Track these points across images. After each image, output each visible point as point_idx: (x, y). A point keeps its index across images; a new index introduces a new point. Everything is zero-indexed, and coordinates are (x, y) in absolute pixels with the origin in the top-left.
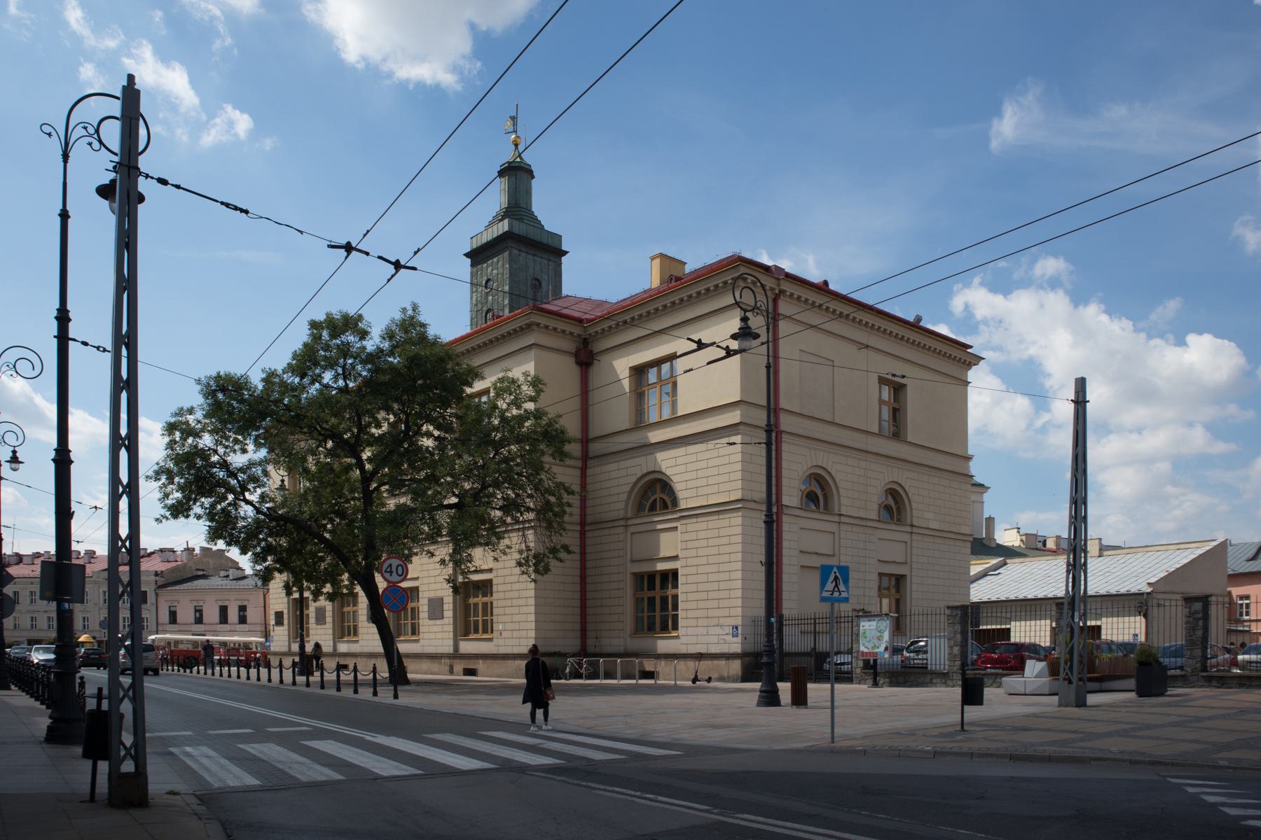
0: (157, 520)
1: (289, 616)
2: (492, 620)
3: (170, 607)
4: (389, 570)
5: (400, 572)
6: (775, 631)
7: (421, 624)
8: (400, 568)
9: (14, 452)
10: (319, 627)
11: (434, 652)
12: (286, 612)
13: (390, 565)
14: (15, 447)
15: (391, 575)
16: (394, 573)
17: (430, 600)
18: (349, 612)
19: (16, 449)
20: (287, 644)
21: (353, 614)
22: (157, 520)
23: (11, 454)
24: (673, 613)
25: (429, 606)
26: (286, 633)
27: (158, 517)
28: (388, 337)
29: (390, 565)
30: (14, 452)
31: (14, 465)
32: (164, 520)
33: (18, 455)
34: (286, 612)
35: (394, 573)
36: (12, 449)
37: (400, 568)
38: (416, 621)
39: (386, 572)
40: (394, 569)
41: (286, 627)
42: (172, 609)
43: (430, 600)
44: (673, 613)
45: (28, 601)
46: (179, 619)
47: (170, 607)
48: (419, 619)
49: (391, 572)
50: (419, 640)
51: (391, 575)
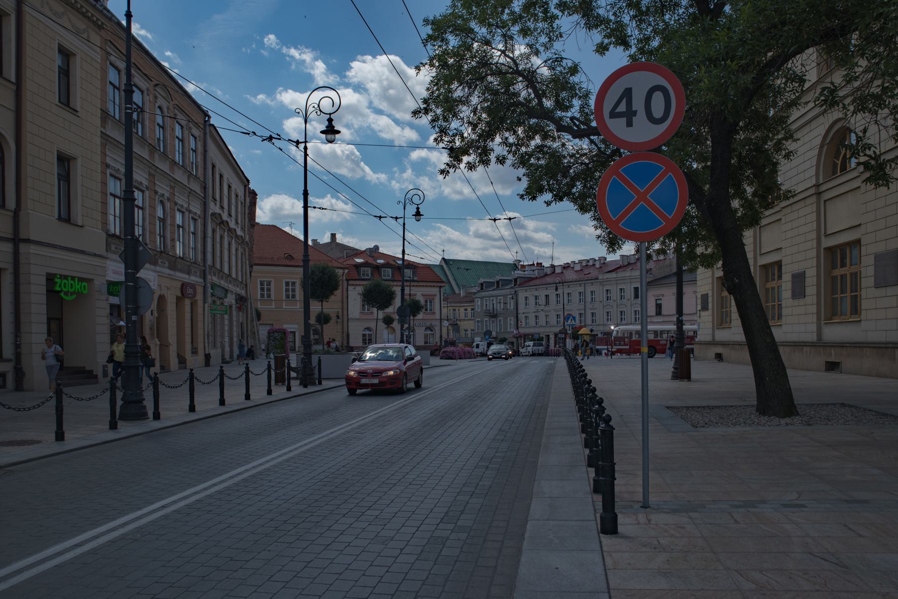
0: (442, 172)
1: (713, 299)
2: (731, 311)
3: (656, 300)
4: (622, 108)
5: (658, 112)
6: (219, 326)
7: (863, 296)
8: (658, 97)
9: (418, 208)
10: (796, 302)
11: (883, 340)
12: (710, 294)
13: (628, 94)
14: (418, 205)
15: (629, 124)
16: (640, 118)
17: (878, 257)
18: (773, 288)
19: (332, 116)
20: (711, 332)
21: (778, 289)
22: (442, 172)
23: (327, 123)
24: (842, 295)
25: (876, 266)
26: (710, 319)
27: (443, 167)
28: (875, 21)
29: (628, 94)
30: (418, 208)
31: (330, 137)
32: (451, 170)
33: (420, 210)
34: (710, 294)
35: (640, 118)
37: (658, 97)
38: (728, 309)
39: (614, 115)
40: (638, 104)
41: (709, 312)
42: (659, 302)
43: (878, 257)
44: (842, 295)
45: (555, 302)
46: (664, 312)
47: (656, 300)
48: (730, 308)
49: (629, 116)
50: (860, 321)
51: (629, 124)
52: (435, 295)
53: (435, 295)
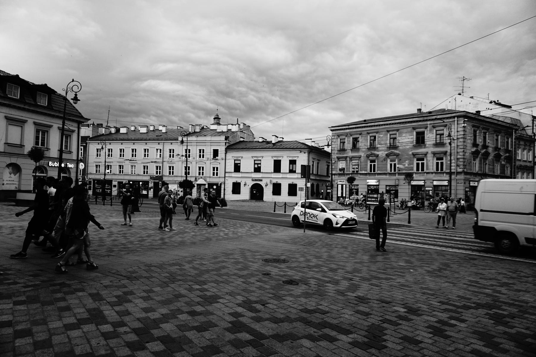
9: (76, 95)
14: (76, 92)
23: (74, 96)
30: (76, 95)
36: (75, 93)
52: (73, 131)
53: (73, 131)
